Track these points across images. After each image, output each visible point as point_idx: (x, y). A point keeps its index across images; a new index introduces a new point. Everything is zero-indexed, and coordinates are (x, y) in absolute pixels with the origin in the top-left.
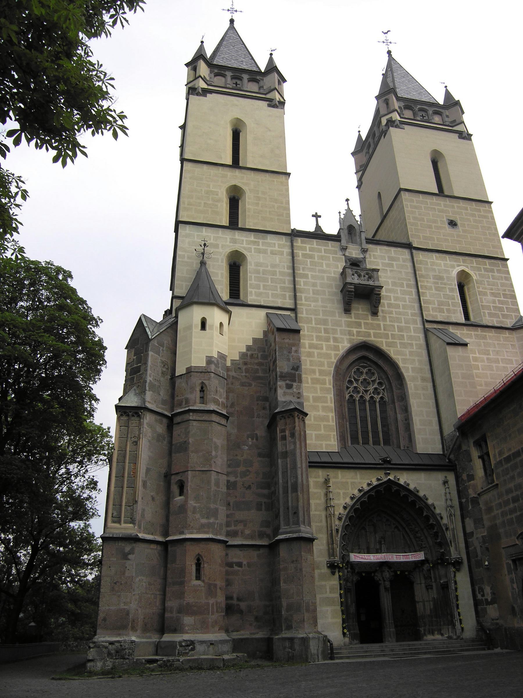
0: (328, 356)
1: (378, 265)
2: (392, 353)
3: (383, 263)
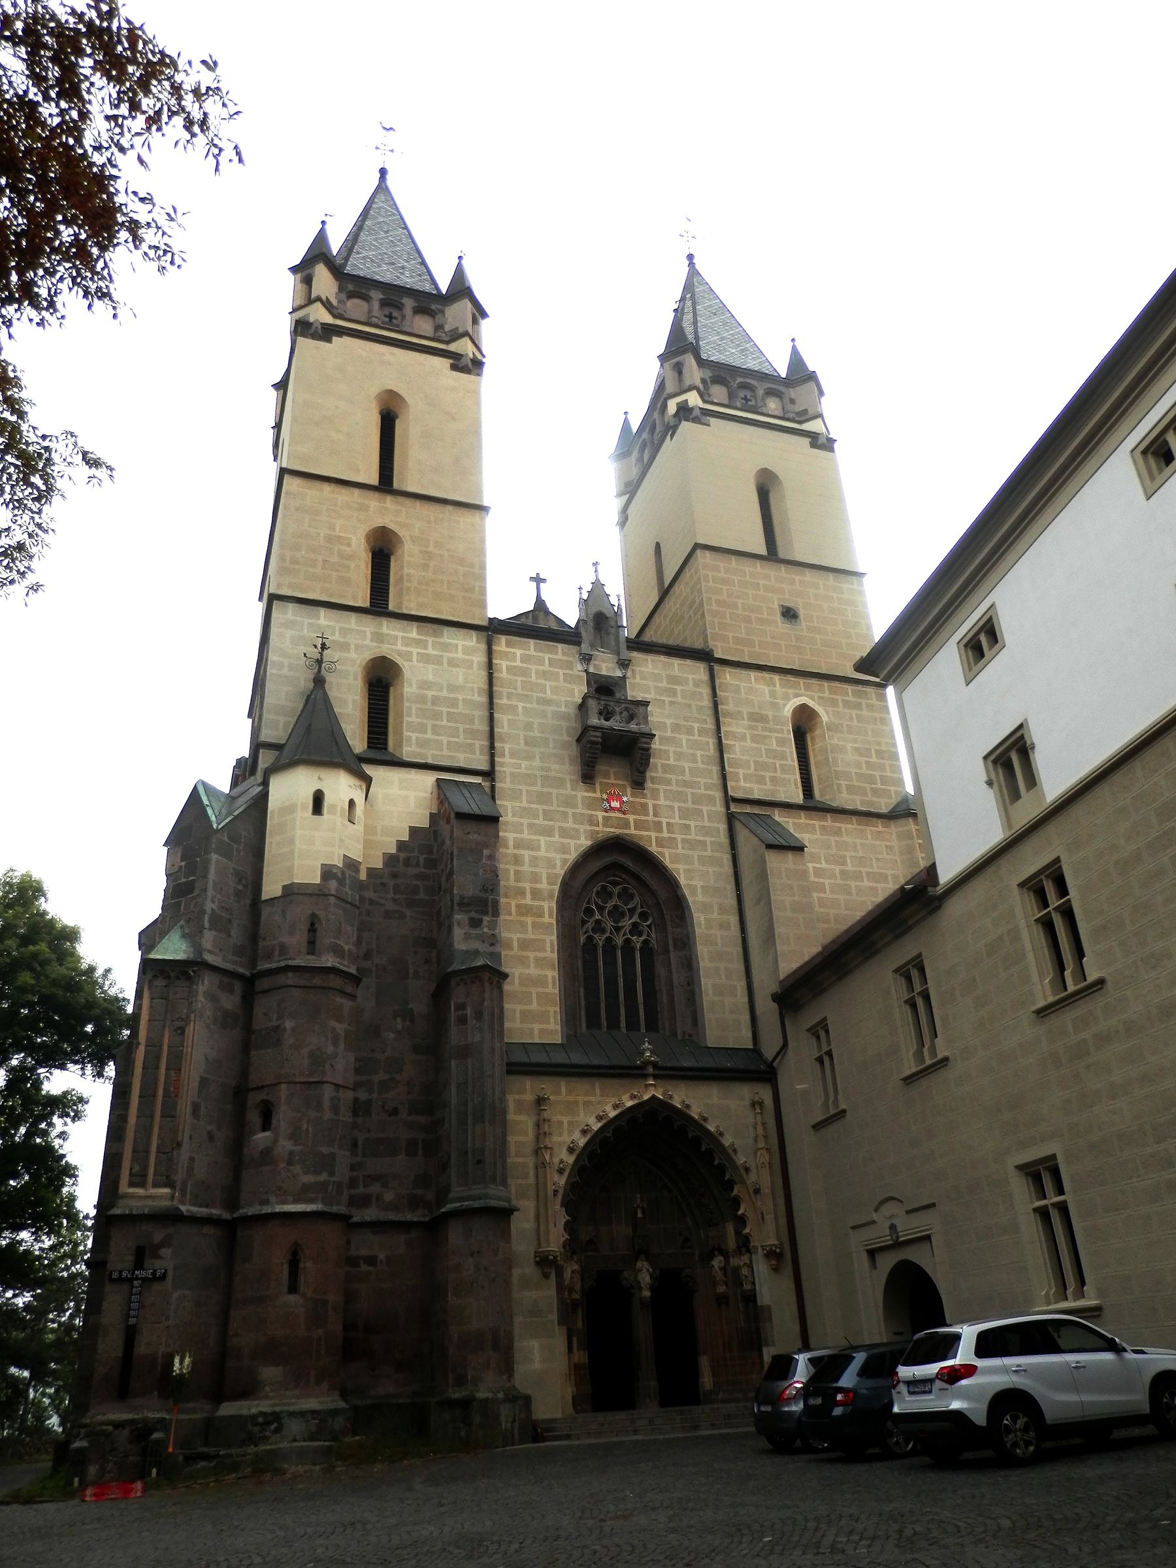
0: (550, 863)
1: (648, 691)
2: (667, 857)
3: (657, 688)
